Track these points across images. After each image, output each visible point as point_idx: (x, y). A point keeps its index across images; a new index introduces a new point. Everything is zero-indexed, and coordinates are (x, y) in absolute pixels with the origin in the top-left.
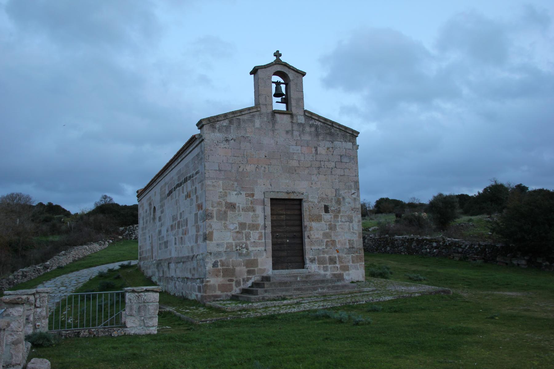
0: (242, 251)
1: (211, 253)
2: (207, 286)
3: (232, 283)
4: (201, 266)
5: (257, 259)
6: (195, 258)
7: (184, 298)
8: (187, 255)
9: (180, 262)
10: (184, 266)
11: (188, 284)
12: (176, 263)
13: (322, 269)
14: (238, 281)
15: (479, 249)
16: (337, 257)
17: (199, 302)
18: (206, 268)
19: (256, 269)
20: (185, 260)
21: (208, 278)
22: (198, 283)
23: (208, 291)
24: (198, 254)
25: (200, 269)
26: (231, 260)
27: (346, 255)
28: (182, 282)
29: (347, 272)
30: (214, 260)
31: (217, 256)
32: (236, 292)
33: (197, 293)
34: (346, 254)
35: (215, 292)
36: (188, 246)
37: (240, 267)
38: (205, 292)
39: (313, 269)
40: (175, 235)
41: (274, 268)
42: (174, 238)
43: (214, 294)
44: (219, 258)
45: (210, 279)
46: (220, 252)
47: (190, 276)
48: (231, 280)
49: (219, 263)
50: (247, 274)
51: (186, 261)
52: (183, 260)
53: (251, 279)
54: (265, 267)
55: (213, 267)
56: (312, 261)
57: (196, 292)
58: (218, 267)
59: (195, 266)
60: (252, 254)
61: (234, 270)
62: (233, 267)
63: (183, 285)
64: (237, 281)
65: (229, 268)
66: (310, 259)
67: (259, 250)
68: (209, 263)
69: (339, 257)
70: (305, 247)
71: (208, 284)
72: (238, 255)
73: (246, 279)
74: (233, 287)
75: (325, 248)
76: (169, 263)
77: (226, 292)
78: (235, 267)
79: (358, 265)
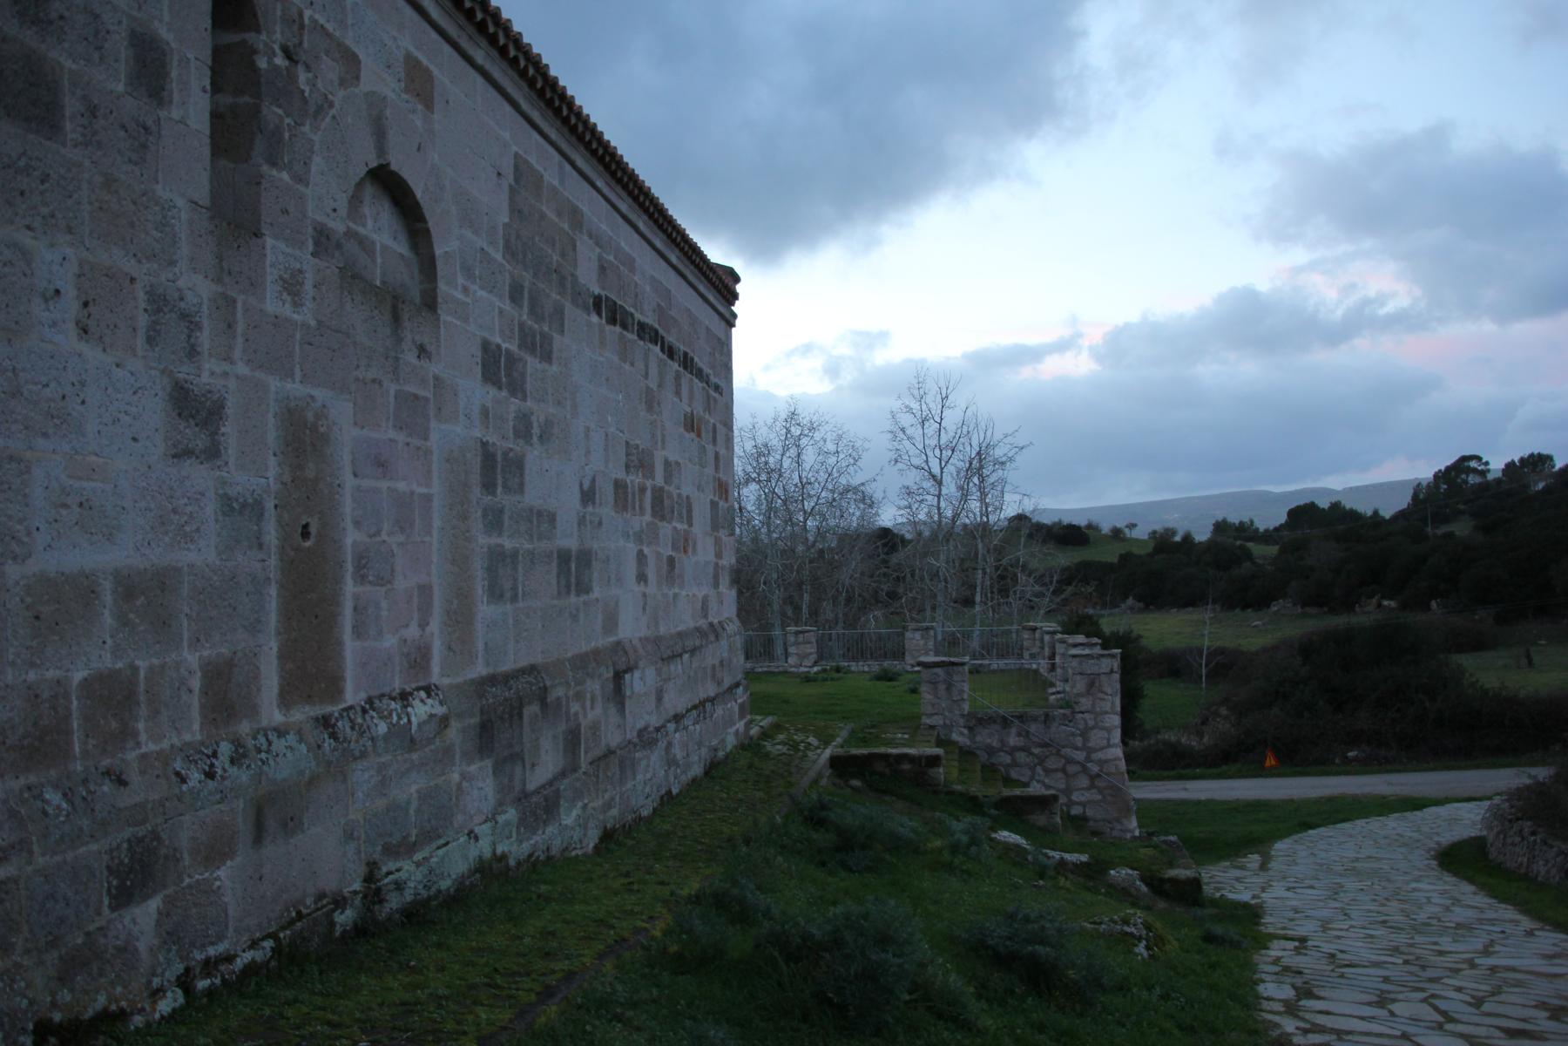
12: (663, 660)
36: (694, 595)
40: (639, 538)
42: (632, 548)
52: (689, 643)
59: (725, 655)
76: (618, 677)
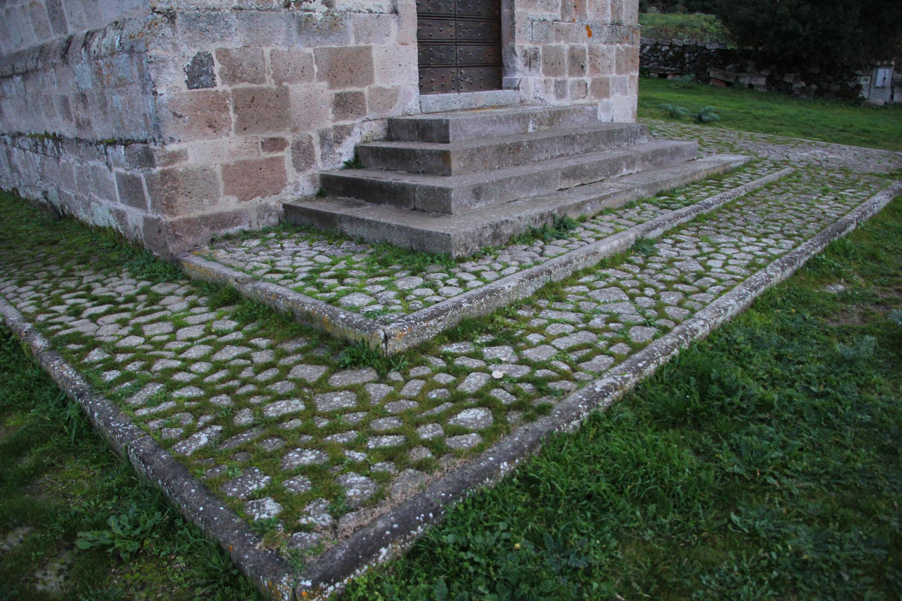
0: (306, 10)
1: (170, 16)
2: (175, 180)
3: (280, 154)
4: (122, 83)
5: (369, 49)
6: (77, 50)
7: (57, 212)
8: (36, 41)
9: (11, 76)
10: (29, 91)
11: (62, 161)
13: (552, 89)
14: (301, 142)
15: (671, 53)
16: (587, 50)
17: (138, 245)
18: (159, 92)
19: (366, 90)
20: (31, 65)
21: (172, 140)
22: (118, 164)
23: (180, 200)
24: (91, 29)
25: (117, 100)
26: (267, 51)
27: (605, 47)
28: (37, 152)
29: (605, 100)
30: (192, 52)
31: (203, 31)
32: (300, 193)
33: (121, 207)
34: (605, 43)
35: (214, 202)
37: (305, 83)
38: (169, 206)
39: (532, 89)
41: (424, 88)
43: (208, 211)
44: (214, 41)
45: (183, 146)
46: (214, 9)
47: (67, 130)
48: (276, 144)
49: (217, 68)
50: (333, 112)
51: (36, 69)
52: (20, 65)
53: (348, 131)
54: (396, 84)
55: (190, 84)
56: (531, 60)
57: (111, 198)
58: (215, 85)
60: (350, 24)
61: (282, 95)
62: (279, 83)
63: (42, 164)
64: (297, 146)
65: (263, 90)
66: (525, 53)
67: (374, 10)
68: (171, 64)
69: (591, 49)
70: (512, 8)
71: (179, 167)
72: (294, 26)
73: (332, 134)
74: (284, 172)
75: (559, 18)
77: (259, 198)
78: (285, 84)
79: (628, 79)
